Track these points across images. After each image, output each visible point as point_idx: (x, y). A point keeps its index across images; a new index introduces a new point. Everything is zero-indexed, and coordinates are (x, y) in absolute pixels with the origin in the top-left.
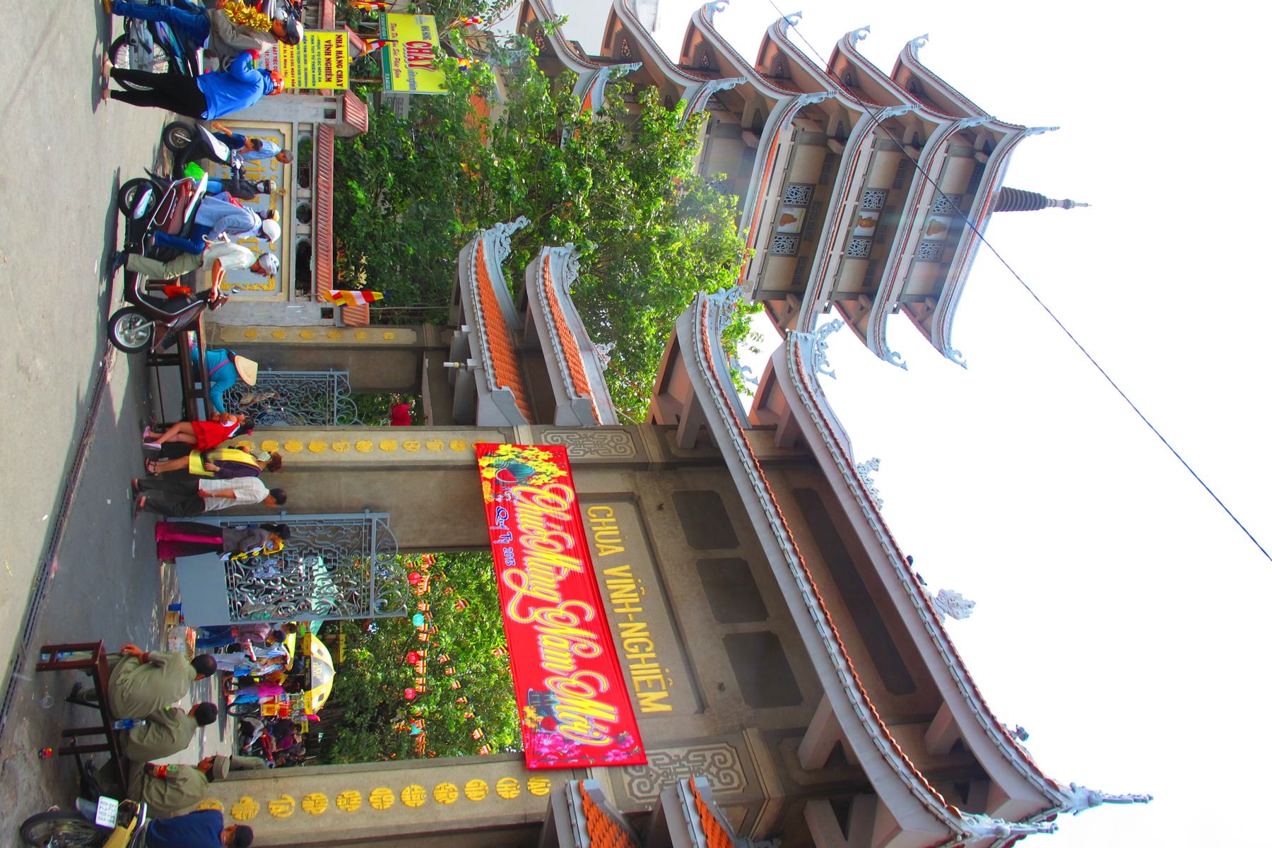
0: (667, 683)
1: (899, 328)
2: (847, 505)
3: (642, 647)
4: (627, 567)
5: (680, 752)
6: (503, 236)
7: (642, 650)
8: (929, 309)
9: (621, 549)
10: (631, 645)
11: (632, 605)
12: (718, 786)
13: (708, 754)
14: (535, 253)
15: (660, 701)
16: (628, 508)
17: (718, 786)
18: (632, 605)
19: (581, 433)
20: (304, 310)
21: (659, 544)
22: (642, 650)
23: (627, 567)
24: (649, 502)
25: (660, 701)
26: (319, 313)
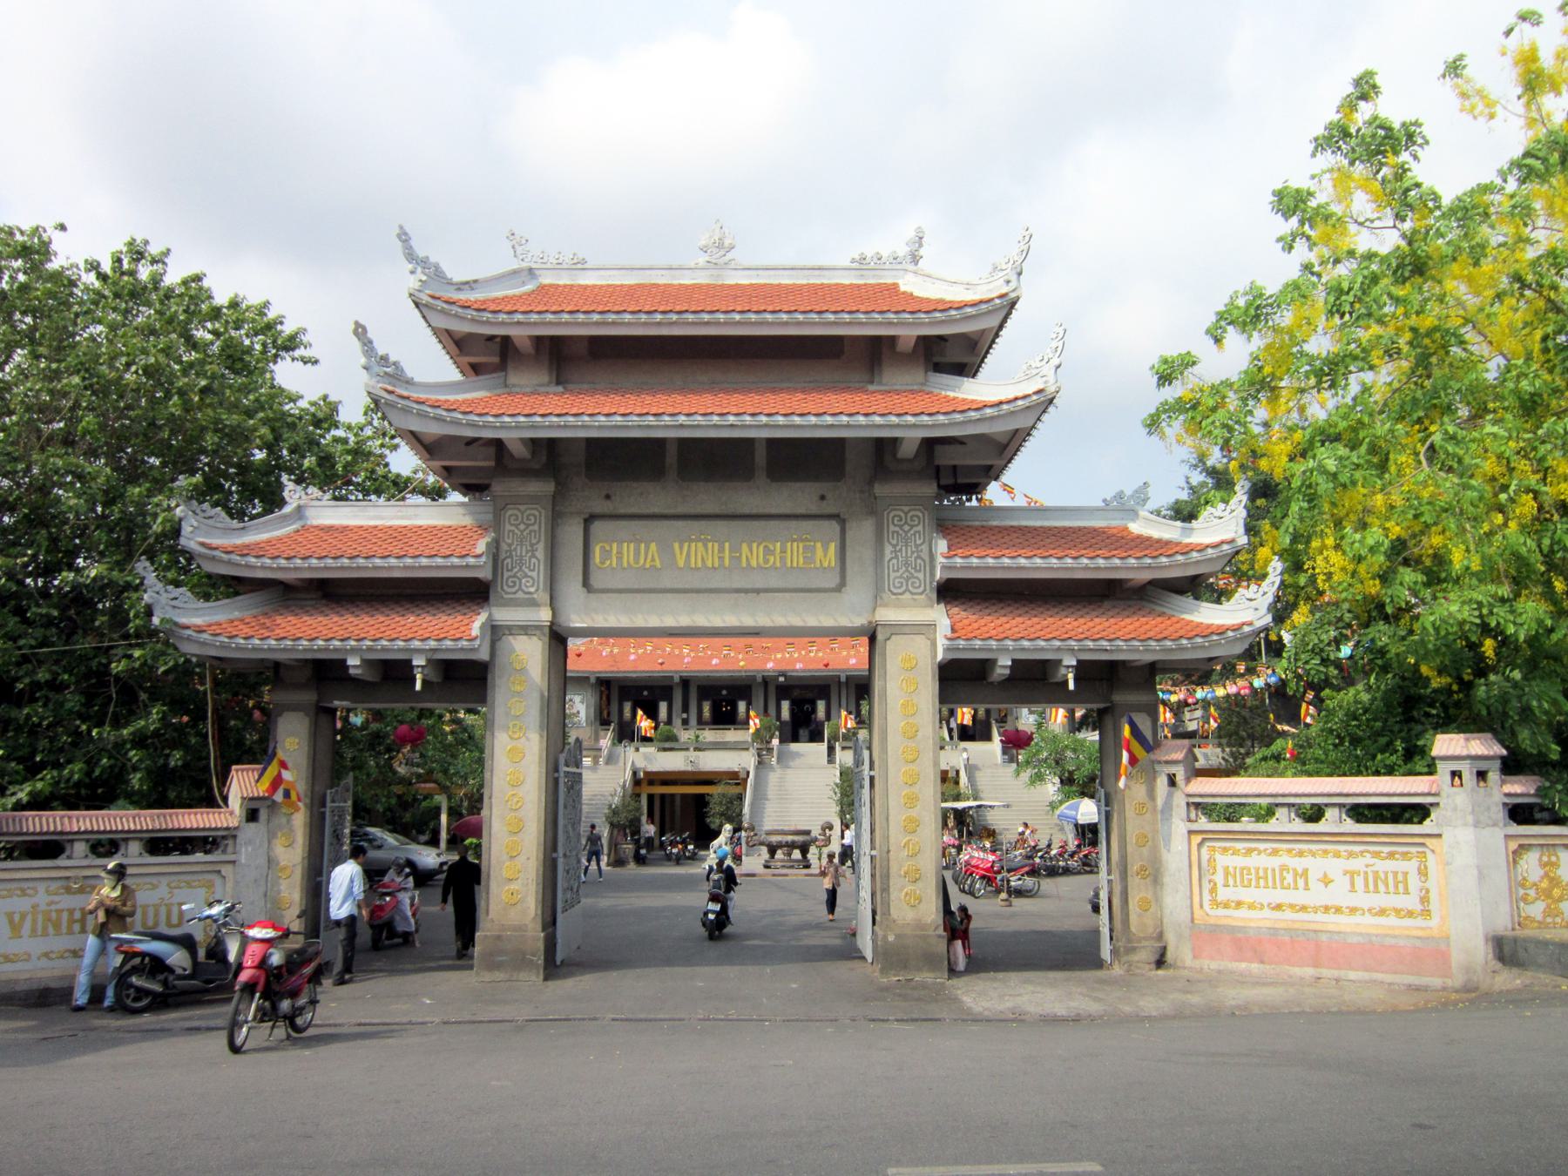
0: (807, 540)
1: (994, 384)
2: (665, 332)
3: (768, 552)
4: (676, 545)
5: (888, 550)
6: (165, 595)
7: (773, 553)
8: (954, 351)
9: (653, 546)
10: (766, 561)
11: (721, 550)
12: (920, 528)
13: (892, 528)
14: (190, 557)
15: (826, 550)
16: (597, 526)
17: (920, 528)
18: (721, 550)
19: (502, 555)
20: (249, 842)
21: (656, 510)
22: (773, 553)
23: (676, 545)
24: (599, 506)
25: (826, 550)
26: (252, 825)
